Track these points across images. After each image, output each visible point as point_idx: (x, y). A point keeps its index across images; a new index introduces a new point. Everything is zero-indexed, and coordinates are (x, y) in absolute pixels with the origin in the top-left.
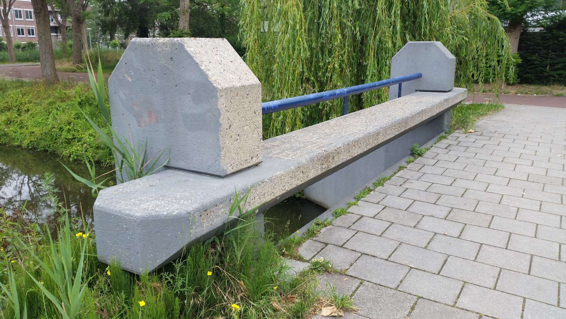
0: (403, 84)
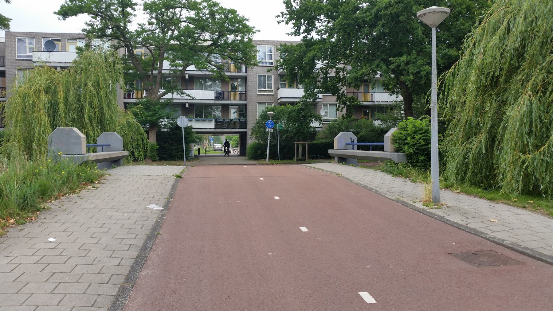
0: (104, 147)
